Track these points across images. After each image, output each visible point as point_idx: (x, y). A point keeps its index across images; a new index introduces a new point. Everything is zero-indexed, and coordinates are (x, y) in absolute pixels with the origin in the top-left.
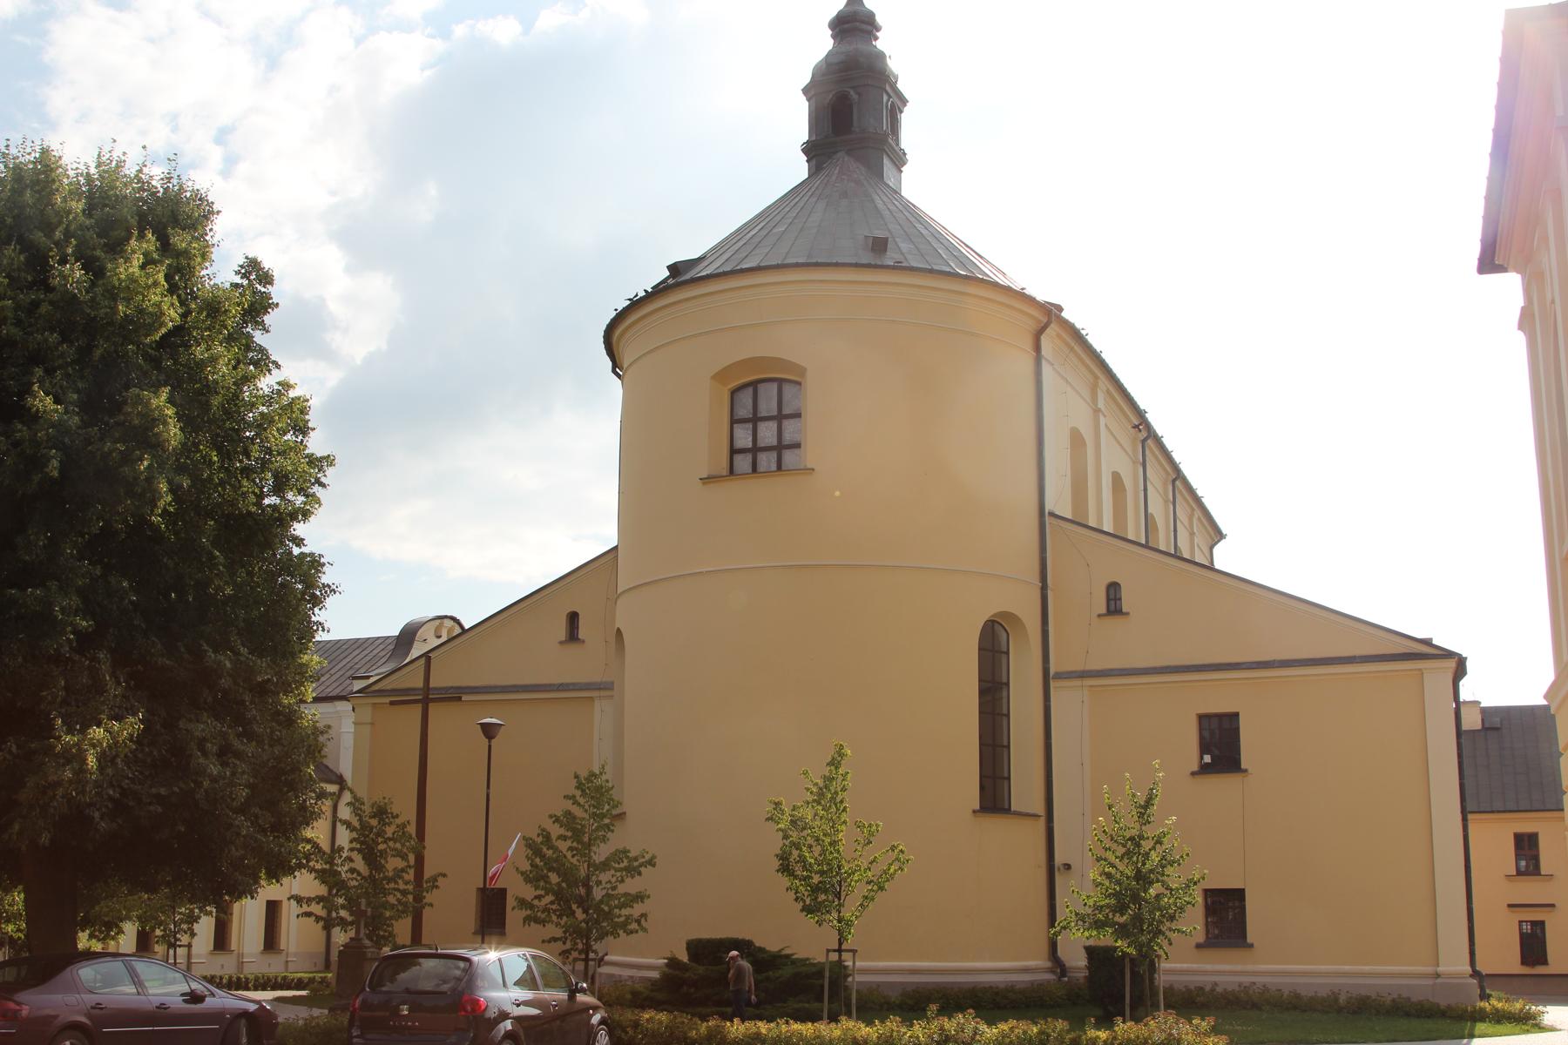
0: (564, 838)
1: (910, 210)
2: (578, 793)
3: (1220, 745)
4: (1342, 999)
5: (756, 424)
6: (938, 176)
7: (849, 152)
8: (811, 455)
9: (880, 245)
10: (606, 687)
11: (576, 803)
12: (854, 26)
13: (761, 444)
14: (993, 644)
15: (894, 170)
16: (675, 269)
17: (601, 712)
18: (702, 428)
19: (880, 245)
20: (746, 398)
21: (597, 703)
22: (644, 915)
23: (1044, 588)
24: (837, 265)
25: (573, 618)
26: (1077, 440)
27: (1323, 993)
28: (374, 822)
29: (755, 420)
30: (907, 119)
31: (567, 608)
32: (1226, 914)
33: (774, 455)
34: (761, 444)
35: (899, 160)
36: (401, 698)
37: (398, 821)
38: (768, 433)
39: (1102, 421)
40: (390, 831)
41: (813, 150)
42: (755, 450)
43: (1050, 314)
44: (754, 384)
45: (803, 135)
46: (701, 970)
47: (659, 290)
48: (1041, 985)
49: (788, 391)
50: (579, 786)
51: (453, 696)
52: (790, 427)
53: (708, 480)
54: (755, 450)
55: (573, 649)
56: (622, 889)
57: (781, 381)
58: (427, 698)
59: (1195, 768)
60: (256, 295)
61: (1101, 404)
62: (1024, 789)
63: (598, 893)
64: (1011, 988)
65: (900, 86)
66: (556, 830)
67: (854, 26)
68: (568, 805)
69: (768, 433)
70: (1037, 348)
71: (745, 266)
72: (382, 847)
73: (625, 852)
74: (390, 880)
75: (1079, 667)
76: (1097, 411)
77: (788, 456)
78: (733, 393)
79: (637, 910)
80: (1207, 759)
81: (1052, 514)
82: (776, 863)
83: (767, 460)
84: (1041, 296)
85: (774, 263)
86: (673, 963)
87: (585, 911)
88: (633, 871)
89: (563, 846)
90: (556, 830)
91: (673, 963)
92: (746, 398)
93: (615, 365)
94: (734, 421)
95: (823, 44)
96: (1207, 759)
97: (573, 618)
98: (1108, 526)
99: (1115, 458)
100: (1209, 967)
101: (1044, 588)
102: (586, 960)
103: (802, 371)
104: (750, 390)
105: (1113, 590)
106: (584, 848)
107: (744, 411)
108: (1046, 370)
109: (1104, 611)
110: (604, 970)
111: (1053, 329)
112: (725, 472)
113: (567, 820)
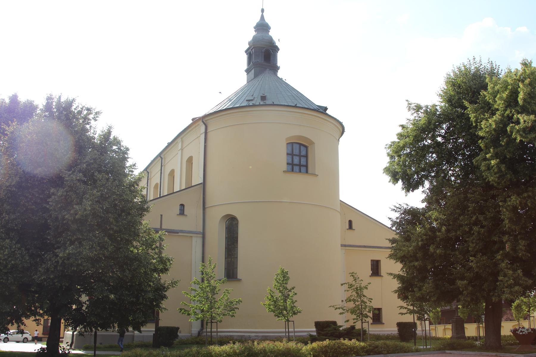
12: (262, 27)
52: (290, 161)
67: (262, 27)
94: (306, 156)
95: (251, 34)
105: (350, 222)
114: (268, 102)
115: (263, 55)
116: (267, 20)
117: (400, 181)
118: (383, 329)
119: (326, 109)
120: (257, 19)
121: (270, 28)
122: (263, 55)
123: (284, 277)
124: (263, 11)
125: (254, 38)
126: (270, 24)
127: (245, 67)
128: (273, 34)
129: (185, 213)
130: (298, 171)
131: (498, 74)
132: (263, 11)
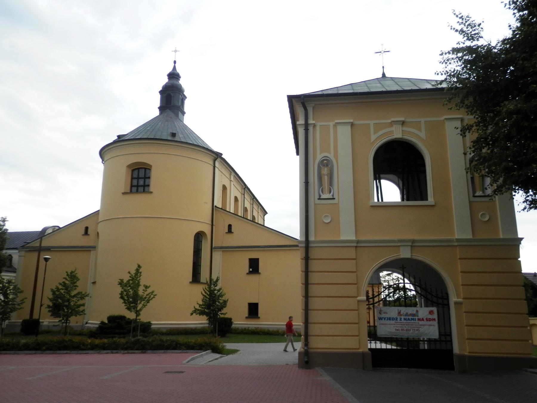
0: (63, 289)
1: (186, 127)
2: (67, 277)
3: (254, 266)
4: (280, 331)
5: (139, 179)
6: (196, 119)
7: (170, 109)
8: (152, 189)
9: (174, 135)
10: (94, 247)
11: (67, 280)
12: (174, 76)
14: (199, 237)
16: (119, 137)
17: (93, 253)
18: (123, 180)
19: (174, 135)
21: (92, 252)
22: (84, 310)
23: (212, 225)
25: (87, 228)
26: (224, 188)
27: (275, 330)
28: (7, 285)
29: (138, 178)
30: (186, 102)
31: (86, 226)
32: (253, 310)
33: (142, 188)
35: (183, 113)
36: (32, 250)
37: (14, 284)
38: (141, 182)
39: (232, 183)
40: (11, 287)
41: (161, 108)
42: (138, 186)
43: (217, 156)
44: (139, 169)
45: (159, 105)
46: (110, 324)
47: (115, 142)
48: (204, 327)
49: (147, 171)
50: (68, 275)
51: (48, 249)
52: (147, 180)
54: (138, 186)
55: (86, 237)
56: (79, 303)
57: (145, 169)
58: (40, 250)
59: (248, 272)
61: (232, 179)
62: (204, 276)
63: (72, 304)
64: (196, 329)
65: (185, 93)
66: (60, 287)
67: (174, 76)
68: (64, 280)
69: (141, 182)
70: (214, 164)
71: (137, 138)
72: (8, 292)
73: (81, 293)
74: (10, 301)
76: (231, 181)
77: (146, 188)
79: (81, 309)
80: (251, 270)
81: (216, 206)
82: (120, 296)
84: (216, 149)
85: (145, 137)
86: (102, 323)
87: (67, 309)
88: (82, 298)
89: (62, 291)
90: (60, 287)
91: (102, 323)
93: (103, 160)
94: (132, 178)
95: (165, 80)
96: (251, 270)
97: (87, 228)
98: (232, 211)
99: (234, 191)
100: (249, 323)
102: (66, 323)
103: (151, 166)
104: (137, 171)
105: (230, 226)
106: (69, 292)
107: (135, 176)
108: (217, 170)
109: (227, 231)
110: (87, 325)
111: (219, 160)
112: (129, 191)
113: (64, 284)
114: (177, 139)
115: (172, 96)
116: (179, 70)
117: (107, 322)
118: (259, 323)
119: (222, 154)
120: (170, 70)
121: (180, 77)
122: (172, 96)
123: (464, 133)
124: (175, 62)
125: (167, 83)
126: (180, 74)
127: (158, 104)
129: (89, 233)
130: (142, 190)
131: (77, 311)
132: (175, 62)
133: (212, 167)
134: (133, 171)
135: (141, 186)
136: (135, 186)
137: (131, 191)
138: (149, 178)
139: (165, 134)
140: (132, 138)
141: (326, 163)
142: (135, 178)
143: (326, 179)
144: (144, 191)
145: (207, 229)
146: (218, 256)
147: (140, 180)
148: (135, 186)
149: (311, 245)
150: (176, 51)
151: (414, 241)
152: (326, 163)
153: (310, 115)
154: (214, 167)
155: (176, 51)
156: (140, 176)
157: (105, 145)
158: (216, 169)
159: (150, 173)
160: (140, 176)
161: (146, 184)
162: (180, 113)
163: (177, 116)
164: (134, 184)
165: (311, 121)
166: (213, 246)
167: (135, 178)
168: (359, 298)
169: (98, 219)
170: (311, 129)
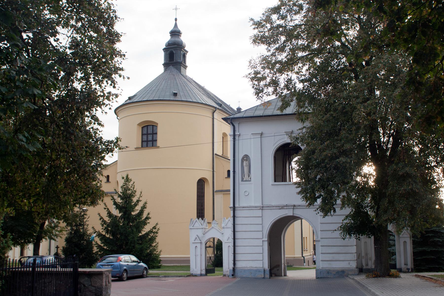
8: (159, 143)
9: (175, 94)
12: (175, 33)
13: (149, 140)
14: (201, 183)
15: (184, 69)
16: (130, 98)
20: (145, 129)
23: (213, 171)
24: (165, 100)
29: (147, 134)
30: (188, 56)
34: (149, 140)
35: (185, 67)
38: (150, 138)
41: (166, 65)
42: (147, 141)
45: (163, 63)
49: (155, 128)
53: (137, 149)
54: (147, 141)
57: (153, 125)
60: (154, 231)
67: (175, 33)
69: (150, 138)
75: (221, 189)
77: (154, 142)
78: (142, 128)
81: (216, 154)
83: (150, 143)
92: (145, 129)
94: (143, 135)
95: (168, 38)
101: (213, 171)
103: (157, 124)
104: (146, 127)
107: (145, 132)
109: (226, 176)
112: (140, 146)
114: (178, 98)
116: (180, 28)
120: (171, 28)
124: (176, 20)
127: (162, 61)
128: (184, 38)
129: (110, 181)
130: (151, 145)
132: (176, 20)
133: (211, 119)
134: (143, 128)
135: (150, 141)
136: (145, 141)
137: (142, 146)
138: (156, 134)
139: (168, 93)
140: (140, 100)
141: (246, 158)
142: (145, 134)
143: (246, 169)
144: (153, 146)
145: (209, 177)
146: (219, 198)
147: (149, 136)
148: (145, 141)
149: (236, 209)
150: (176, 9)
151: (294, 206)
152: (246, 158)
153: (237, 129)
154: (213, 119)
155: (176, 9)
156: (149, 132)
157: (117, 107)
158: (215, 120)
159: (157, 129)
160: (149, 132)
161: (154, 139)
162: (182, 68)
163: (180, 71)
164: (144, 140)
165: (237, 133)
166: (215, 190)
167: (145, 134)
168: (264, 239)
169: (116, 169)
170: (237, 138)
